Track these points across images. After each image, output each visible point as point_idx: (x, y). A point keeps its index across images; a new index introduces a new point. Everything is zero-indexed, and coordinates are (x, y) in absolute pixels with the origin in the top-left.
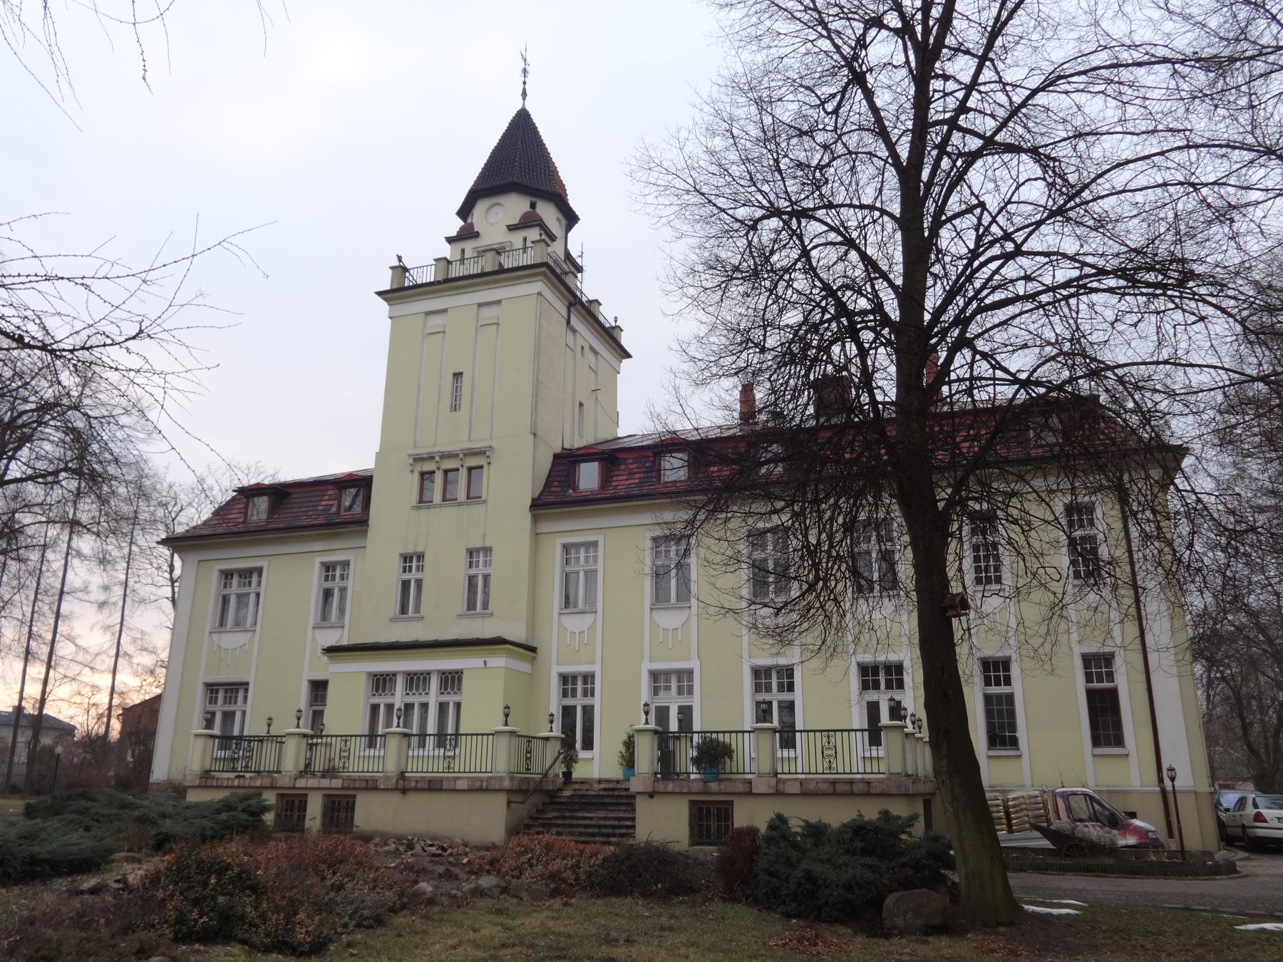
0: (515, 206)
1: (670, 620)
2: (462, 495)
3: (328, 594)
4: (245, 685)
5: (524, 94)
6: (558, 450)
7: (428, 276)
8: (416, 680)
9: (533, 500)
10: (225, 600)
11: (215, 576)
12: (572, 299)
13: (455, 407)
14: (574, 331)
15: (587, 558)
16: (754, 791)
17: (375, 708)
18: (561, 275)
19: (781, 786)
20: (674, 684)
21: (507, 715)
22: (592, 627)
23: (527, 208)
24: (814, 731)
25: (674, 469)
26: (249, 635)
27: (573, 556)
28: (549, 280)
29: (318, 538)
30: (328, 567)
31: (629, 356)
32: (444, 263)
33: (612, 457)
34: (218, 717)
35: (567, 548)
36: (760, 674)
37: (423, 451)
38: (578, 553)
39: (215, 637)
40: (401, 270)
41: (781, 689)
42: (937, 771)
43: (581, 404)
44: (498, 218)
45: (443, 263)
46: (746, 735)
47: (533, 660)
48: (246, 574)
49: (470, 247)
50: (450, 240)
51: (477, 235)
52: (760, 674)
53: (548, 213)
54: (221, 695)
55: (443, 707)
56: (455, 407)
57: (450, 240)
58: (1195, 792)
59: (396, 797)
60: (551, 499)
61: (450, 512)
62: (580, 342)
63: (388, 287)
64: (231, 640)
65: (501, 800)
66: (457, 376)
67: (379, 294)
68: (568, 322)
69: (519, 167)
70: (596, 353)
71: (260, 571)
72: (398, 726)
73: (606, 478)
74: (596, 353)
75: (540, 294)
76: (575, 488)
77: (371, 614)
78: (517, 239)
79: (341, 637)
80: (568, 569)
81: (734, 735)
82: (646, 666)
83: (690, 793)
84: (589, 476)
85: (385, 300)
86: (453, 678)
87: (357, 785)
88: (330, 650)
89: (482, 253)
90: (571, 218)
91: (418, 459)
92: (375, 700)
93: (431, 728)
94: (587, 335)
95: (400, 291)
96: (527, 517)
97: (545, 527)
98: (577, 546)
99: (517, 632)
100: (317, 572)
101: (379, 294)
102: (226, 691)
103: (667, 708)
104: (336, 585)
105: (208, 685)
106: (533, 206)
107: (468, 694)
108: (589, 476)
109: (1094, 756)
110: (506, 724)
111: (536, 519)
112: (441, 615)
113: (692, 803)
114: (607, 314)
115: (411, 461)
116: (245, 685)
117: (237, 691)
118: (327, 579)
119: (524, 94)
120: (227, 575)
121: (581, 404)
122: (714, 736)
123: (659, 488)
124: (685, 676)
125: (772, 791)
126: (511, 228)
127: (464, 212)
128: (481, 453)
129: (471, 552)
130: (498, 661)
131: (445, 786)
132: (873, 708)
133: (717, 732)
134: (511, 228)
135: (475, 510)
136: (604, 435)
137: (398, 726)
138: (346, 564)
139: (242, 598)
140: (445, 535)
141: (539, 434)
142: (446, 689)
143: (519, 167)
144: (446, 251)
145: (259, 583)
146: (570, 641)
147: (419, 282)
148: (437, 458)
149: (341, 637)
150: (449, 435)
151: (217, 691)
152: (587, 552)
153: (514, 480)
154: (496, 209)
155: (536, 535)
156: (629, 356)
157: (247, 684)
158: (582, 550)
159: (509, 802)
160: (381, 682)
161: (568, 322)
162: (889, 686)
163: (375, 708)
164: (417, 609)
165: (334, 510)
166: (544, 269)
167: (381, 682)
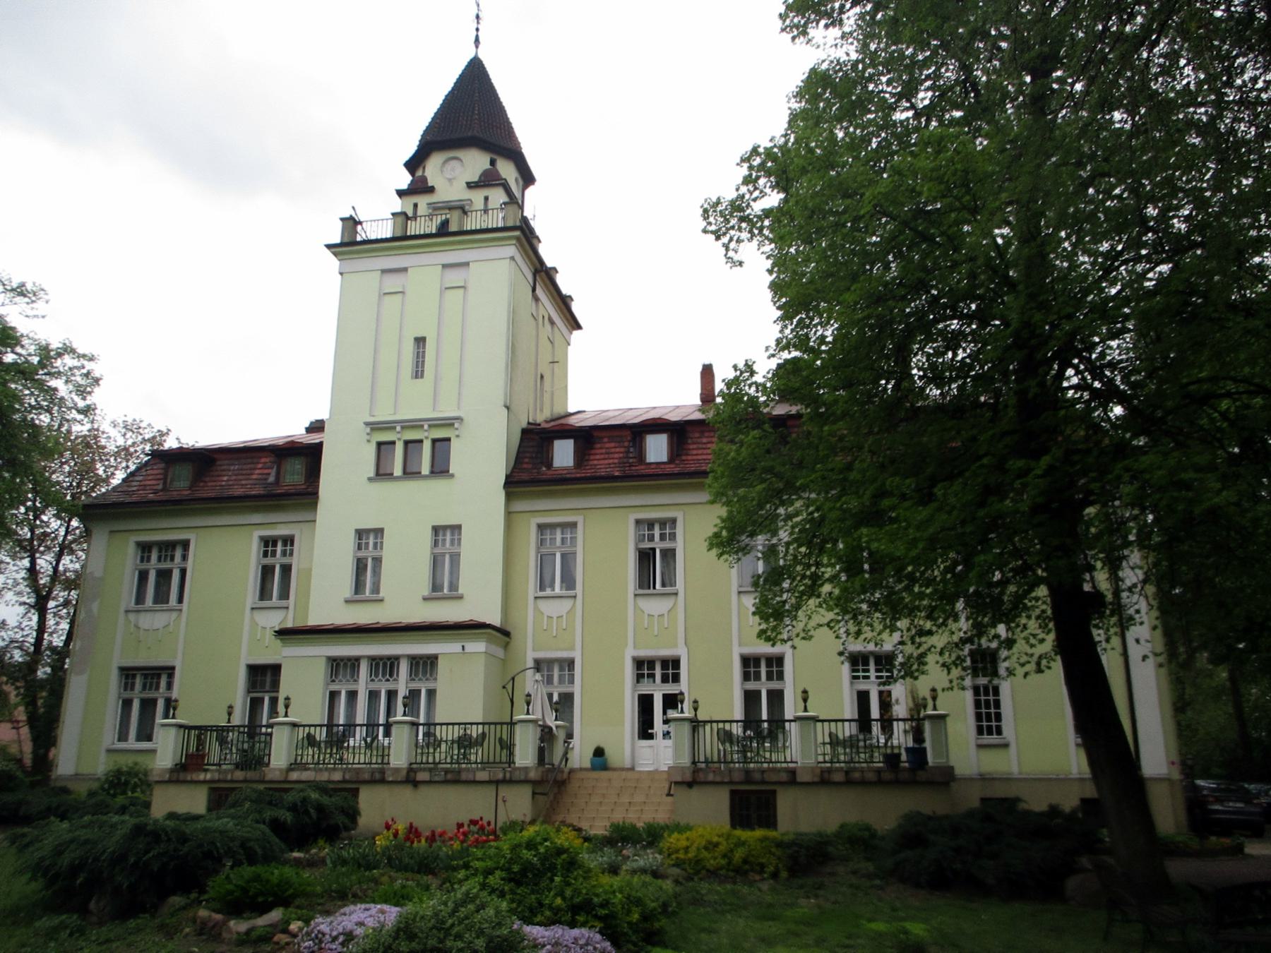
0: (474, 162)
1: (655, 606)
2: (398, 471)
3: (267, 572)
4: (170, 671)
5: (477, 41)
6: (524, 425)
7: (386, 231)
8: (385, 666)
9: (507, 477)
10: (143, 576)
11: (131, 549)
12: (538, 265)
13: (418, 373)
14: (536, 299)
15: (563, 540)
16: (799, 780)
17: (334, 695)
18: (526, 236)
19: (826, 775)
20: (658, 672)
21: (805, 700)
22: (571, 611)
23: (488, 166)
24: (453, 724)
25: (657, 448)
26: (174, 615)
27: (440, 538)
28: (522, 245)
29: (256, 510)
30: (269, 543)
31: (579, 327)
32: (351, 222)
33: (589, 437)
34: (136, 705)
35: (541, 527)
36: (749, 662)
37: (383, 415)
38: (444, 535)
39: (132, 617)
40: (351, 223)
41: (770, 677)
42: (1092, 762)
43: (542, 377)
44: (454, 175)
45: (400, 219)
46: (847, 724)
47: (506, 646)
48: (167, 548)
49: (423, 201)
50: (401, 193)
51: (431, 190)
52: (749, 662)
53: (507, 170)
54: (138, 681)
55: (373, 695)
56: (418, 373)
57: (401, 193)
58: (1169, 780)
59: (407, 791)
60: (525, 477)
61: (412, 486)
62: (542, 311)
63: (337, 240)
64: (155, 620)
65: (526, 791)
66: (420, 341)
67: (329, 246)
68: (534, 290)
69: (471, 118)
70: (552, 322)
71: (185, 544)
72: (405, 715)
73: (581, 455)
74: (552, 322)
75: (512, 258)
76: (549, 464)
77: (326, 595)
78: (477, 197)
79: (285, 617)
80: (544, 550)
81: (840, 724)
82: (630, 653)
83: (731, 783)
84: (564, 454)
85: (335, 254)
86: (385, 665)
87: (774, 778)
88: (283, 633)
89: (435, 208)
90: (528, 178)
91: (375, 427)
92: (334, 687)
93: (361, 717)
94: (548, 307)
95: (350, 244)
96: (501, 495)
97: (520, 506)
98: (552, 526)
99: (496, 620)
100: (255, 547)
101: (329, 246)
102: (146, 676)
103: (652, 696)
104: (278, 561)
105: (123, 670)
106: (493, 163)
107: (444, 680)
108: (564, 454)
109: (980, 746)
110: (806, 710)
111: (509, 497)
112: (404, 597)
113: (733, 793)
114: (565, 284)
115: (368, 430)
116: (170, 671)
117: (159, 676)
118: (265, 554)
119: (477, 41)
120: (145, 548)
121: (542, 377)
122: (727, 726)
123: (642, 469)
124: (671, 667)
125: (816, 779)
126: (470, 186)
127: (413, 164)
128: (449, 423)
129: (436, 530)
130: (477, 646)
131: (464, 776)
132: (863, 697)
133: (724, 722)
134: (470, 186)
135: (439, 484)
136: (558, 410)
137: (405, 715)
138: (289, 541)
139: (164, 575)
140: (408, 511)
141: (512, 407)
142: (377, 676)
143: (471, 118)
144: (397, 205)
145: (185, 558)
146: (547, 624)
147: (373, 237)
148: (398, 428)
149: (285, 617)
150: (416, 403)
151: (134, 676)
152: (453, 534)
153: (484, 456)
154: (453, 163)
155: (509, 514)
156: (579, 327)
157: (173, 668)
158: (558, 532)
159: (534, 794)
160: (338, 666)
161: (534, 290)
162: (665, 679)
163: (334, 695)
164: (376, 590)
165: (271, 479)
166: (517, 233)
167: (338, 666)
